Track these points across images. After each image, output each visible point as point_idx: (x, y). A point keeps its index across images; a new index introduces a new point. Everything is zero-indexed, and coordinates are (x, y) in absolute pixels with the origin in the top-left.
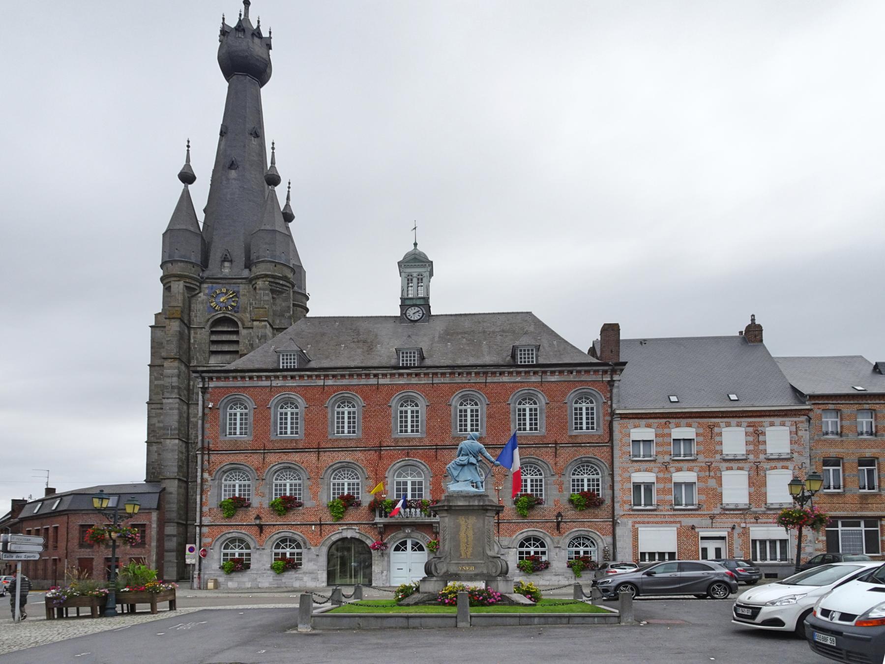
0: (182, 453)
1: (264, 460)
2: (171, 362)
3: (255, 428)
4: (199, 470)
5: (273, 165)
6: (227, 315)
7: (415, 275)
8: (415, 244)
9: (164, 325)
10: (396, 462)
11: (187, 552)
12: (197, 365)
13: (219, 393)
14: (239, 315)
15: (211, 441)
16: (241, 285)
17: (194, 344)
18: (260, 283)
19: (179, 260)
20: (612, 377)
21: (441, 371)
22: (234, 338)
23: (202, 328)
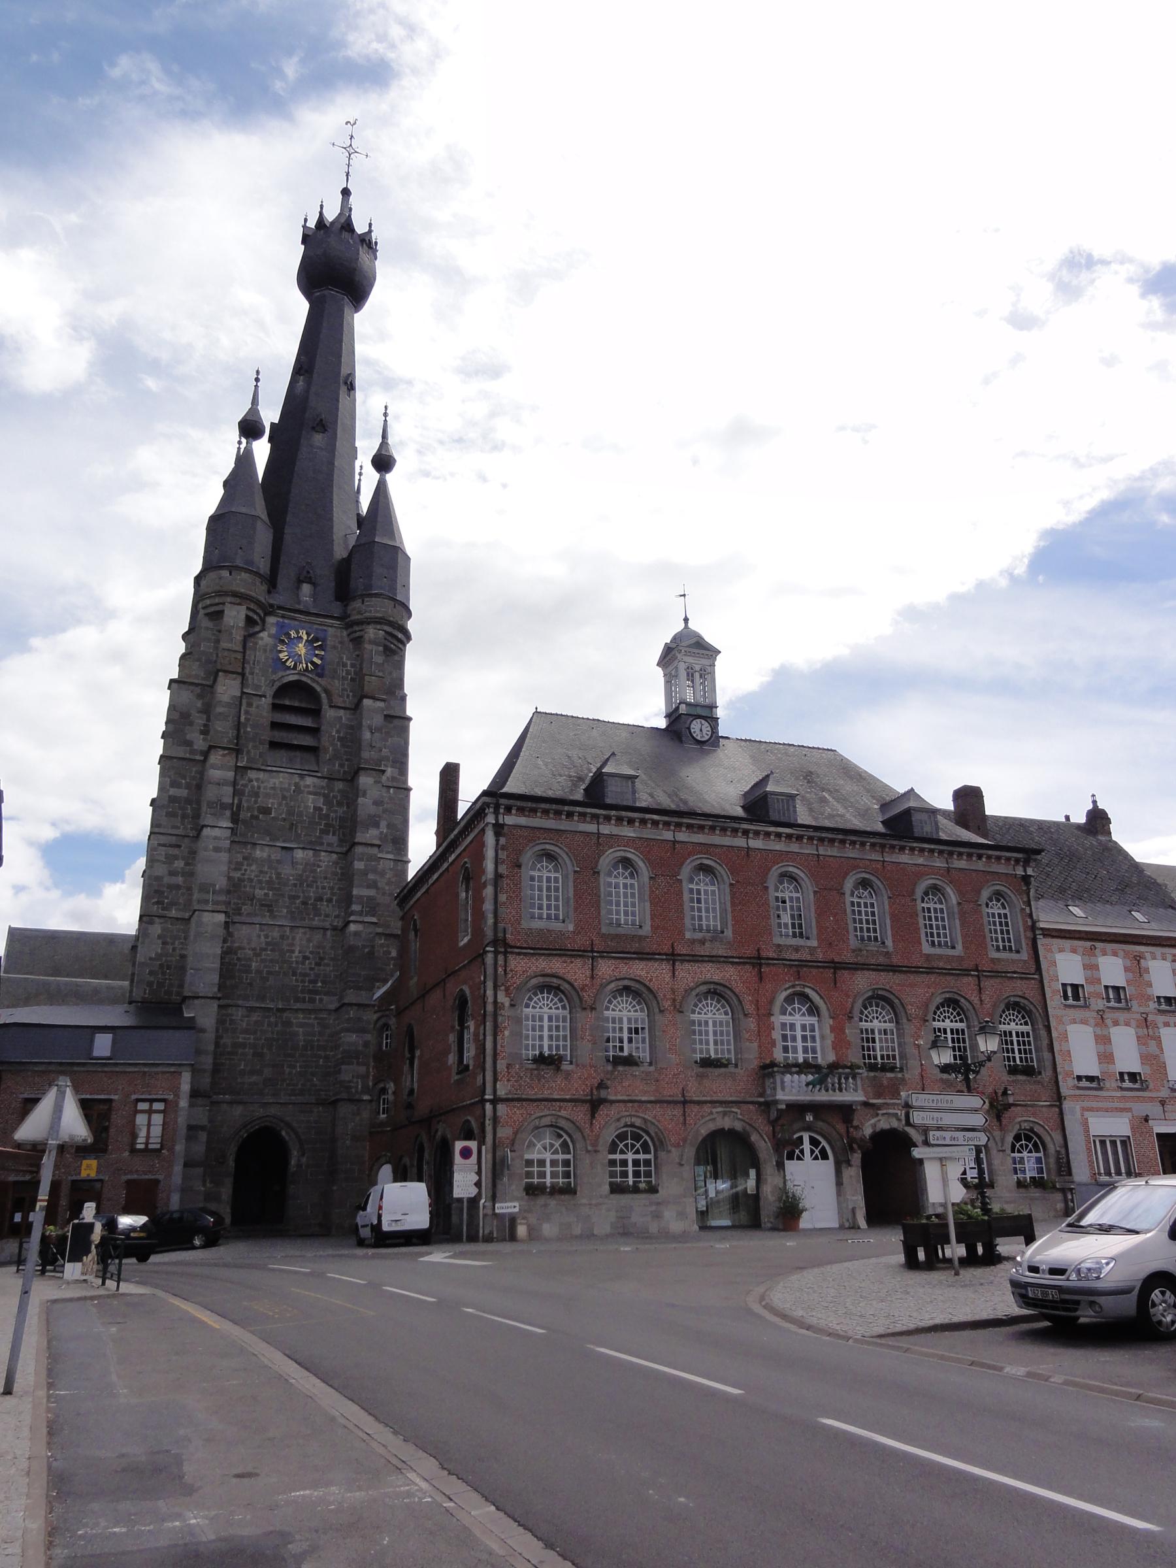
2: (224, 755)
4: (490, 984)
6: (304, 679)
7: (697, 668)
8: (686, 620)
11: (458, 1158)
15: (510, 929)
16: (330, 629)
17: (245, 726)
18: (371, 632)
19: (243, 568)
20: (1025, 871)
21: (754, 828)
22: (307, 722)
23: (261, 696)
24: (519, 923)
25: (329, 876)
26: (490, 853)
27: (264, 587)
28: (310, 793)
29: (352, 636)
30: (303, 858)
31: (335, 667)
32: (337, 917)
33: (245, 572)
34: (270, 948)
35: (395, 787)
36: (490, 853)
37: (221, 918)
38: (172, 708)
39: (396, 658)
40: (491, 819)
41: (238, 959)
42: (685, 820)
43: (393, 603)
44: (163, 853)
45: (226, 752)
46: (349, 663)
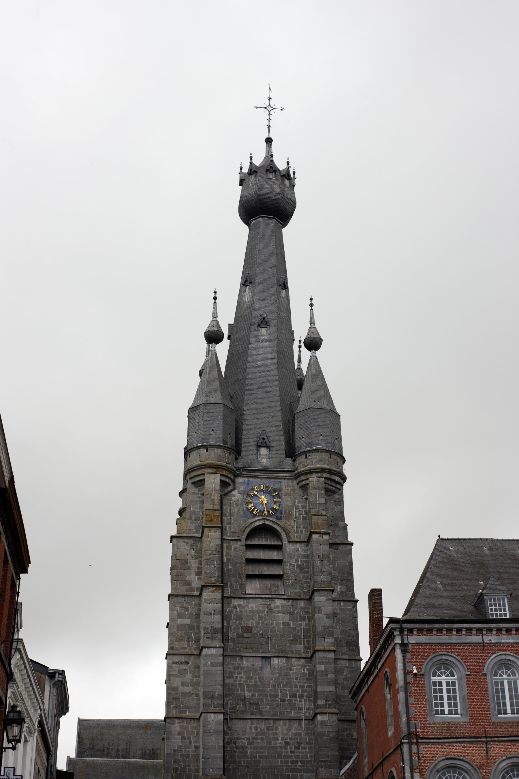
1: (487, 753)
2: (213, 592)
3: (470, 704)
4: (407, 769)
5: (313, 326)
6: (268, 523)
12: (233, 595)
13: (422, 651)
16: (283, 481)
18: (313, 480)
22: (274, 555)
24: (427, 720)
25: (299, 677)
26: (400, 666)
27: (233, 456)
28: (279, 612)
29: (301, 484)
30: (278, 664)
32: (308, 709)
33: (217, 448)
34: (259, 737)
35: (344, 601)
36: (400, 666)
37: (221, 717)
38: (174, 557)
39: (336, 496)
40: (398, 640)
41: (237, 747)
44: (177, 669)
45: (215, 588)
46: (300, 505)
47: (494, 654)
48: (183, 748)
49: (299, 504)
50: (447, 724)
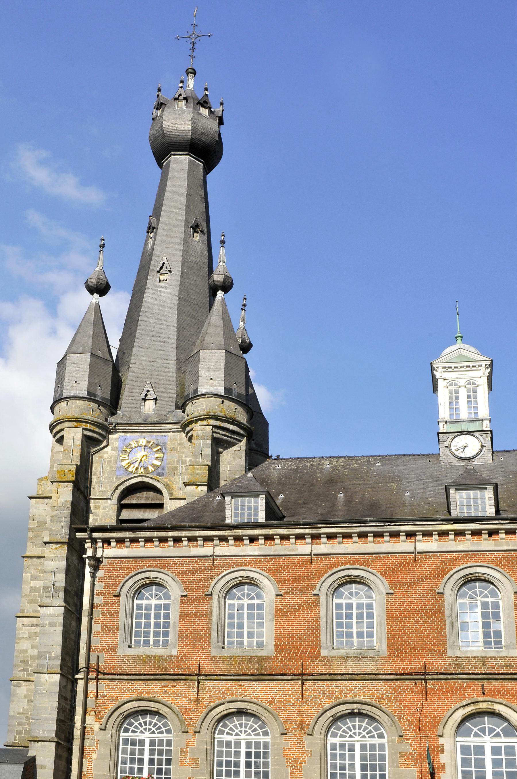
0: (66, 699)
2: (56, 549)
9: (50, 495)
10: (458, 705)
13: (121, 567)
14: (164, 479)
24: (115, 651)
31: (175, 465)
42: (321, 531)
43: (221, 400)
44: (27, 632)
45: (59, 545)
47: (228, 569)
48: (29, 711)
49: (186, 459)
50: (144, 656)
